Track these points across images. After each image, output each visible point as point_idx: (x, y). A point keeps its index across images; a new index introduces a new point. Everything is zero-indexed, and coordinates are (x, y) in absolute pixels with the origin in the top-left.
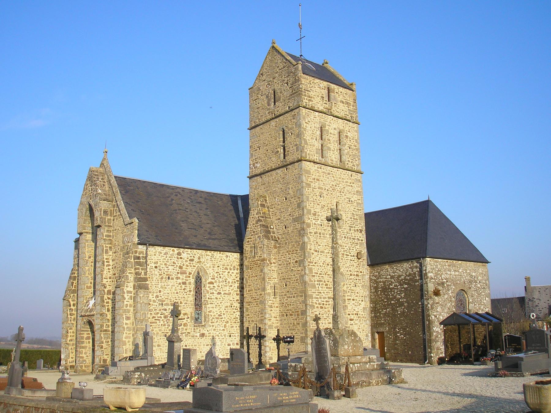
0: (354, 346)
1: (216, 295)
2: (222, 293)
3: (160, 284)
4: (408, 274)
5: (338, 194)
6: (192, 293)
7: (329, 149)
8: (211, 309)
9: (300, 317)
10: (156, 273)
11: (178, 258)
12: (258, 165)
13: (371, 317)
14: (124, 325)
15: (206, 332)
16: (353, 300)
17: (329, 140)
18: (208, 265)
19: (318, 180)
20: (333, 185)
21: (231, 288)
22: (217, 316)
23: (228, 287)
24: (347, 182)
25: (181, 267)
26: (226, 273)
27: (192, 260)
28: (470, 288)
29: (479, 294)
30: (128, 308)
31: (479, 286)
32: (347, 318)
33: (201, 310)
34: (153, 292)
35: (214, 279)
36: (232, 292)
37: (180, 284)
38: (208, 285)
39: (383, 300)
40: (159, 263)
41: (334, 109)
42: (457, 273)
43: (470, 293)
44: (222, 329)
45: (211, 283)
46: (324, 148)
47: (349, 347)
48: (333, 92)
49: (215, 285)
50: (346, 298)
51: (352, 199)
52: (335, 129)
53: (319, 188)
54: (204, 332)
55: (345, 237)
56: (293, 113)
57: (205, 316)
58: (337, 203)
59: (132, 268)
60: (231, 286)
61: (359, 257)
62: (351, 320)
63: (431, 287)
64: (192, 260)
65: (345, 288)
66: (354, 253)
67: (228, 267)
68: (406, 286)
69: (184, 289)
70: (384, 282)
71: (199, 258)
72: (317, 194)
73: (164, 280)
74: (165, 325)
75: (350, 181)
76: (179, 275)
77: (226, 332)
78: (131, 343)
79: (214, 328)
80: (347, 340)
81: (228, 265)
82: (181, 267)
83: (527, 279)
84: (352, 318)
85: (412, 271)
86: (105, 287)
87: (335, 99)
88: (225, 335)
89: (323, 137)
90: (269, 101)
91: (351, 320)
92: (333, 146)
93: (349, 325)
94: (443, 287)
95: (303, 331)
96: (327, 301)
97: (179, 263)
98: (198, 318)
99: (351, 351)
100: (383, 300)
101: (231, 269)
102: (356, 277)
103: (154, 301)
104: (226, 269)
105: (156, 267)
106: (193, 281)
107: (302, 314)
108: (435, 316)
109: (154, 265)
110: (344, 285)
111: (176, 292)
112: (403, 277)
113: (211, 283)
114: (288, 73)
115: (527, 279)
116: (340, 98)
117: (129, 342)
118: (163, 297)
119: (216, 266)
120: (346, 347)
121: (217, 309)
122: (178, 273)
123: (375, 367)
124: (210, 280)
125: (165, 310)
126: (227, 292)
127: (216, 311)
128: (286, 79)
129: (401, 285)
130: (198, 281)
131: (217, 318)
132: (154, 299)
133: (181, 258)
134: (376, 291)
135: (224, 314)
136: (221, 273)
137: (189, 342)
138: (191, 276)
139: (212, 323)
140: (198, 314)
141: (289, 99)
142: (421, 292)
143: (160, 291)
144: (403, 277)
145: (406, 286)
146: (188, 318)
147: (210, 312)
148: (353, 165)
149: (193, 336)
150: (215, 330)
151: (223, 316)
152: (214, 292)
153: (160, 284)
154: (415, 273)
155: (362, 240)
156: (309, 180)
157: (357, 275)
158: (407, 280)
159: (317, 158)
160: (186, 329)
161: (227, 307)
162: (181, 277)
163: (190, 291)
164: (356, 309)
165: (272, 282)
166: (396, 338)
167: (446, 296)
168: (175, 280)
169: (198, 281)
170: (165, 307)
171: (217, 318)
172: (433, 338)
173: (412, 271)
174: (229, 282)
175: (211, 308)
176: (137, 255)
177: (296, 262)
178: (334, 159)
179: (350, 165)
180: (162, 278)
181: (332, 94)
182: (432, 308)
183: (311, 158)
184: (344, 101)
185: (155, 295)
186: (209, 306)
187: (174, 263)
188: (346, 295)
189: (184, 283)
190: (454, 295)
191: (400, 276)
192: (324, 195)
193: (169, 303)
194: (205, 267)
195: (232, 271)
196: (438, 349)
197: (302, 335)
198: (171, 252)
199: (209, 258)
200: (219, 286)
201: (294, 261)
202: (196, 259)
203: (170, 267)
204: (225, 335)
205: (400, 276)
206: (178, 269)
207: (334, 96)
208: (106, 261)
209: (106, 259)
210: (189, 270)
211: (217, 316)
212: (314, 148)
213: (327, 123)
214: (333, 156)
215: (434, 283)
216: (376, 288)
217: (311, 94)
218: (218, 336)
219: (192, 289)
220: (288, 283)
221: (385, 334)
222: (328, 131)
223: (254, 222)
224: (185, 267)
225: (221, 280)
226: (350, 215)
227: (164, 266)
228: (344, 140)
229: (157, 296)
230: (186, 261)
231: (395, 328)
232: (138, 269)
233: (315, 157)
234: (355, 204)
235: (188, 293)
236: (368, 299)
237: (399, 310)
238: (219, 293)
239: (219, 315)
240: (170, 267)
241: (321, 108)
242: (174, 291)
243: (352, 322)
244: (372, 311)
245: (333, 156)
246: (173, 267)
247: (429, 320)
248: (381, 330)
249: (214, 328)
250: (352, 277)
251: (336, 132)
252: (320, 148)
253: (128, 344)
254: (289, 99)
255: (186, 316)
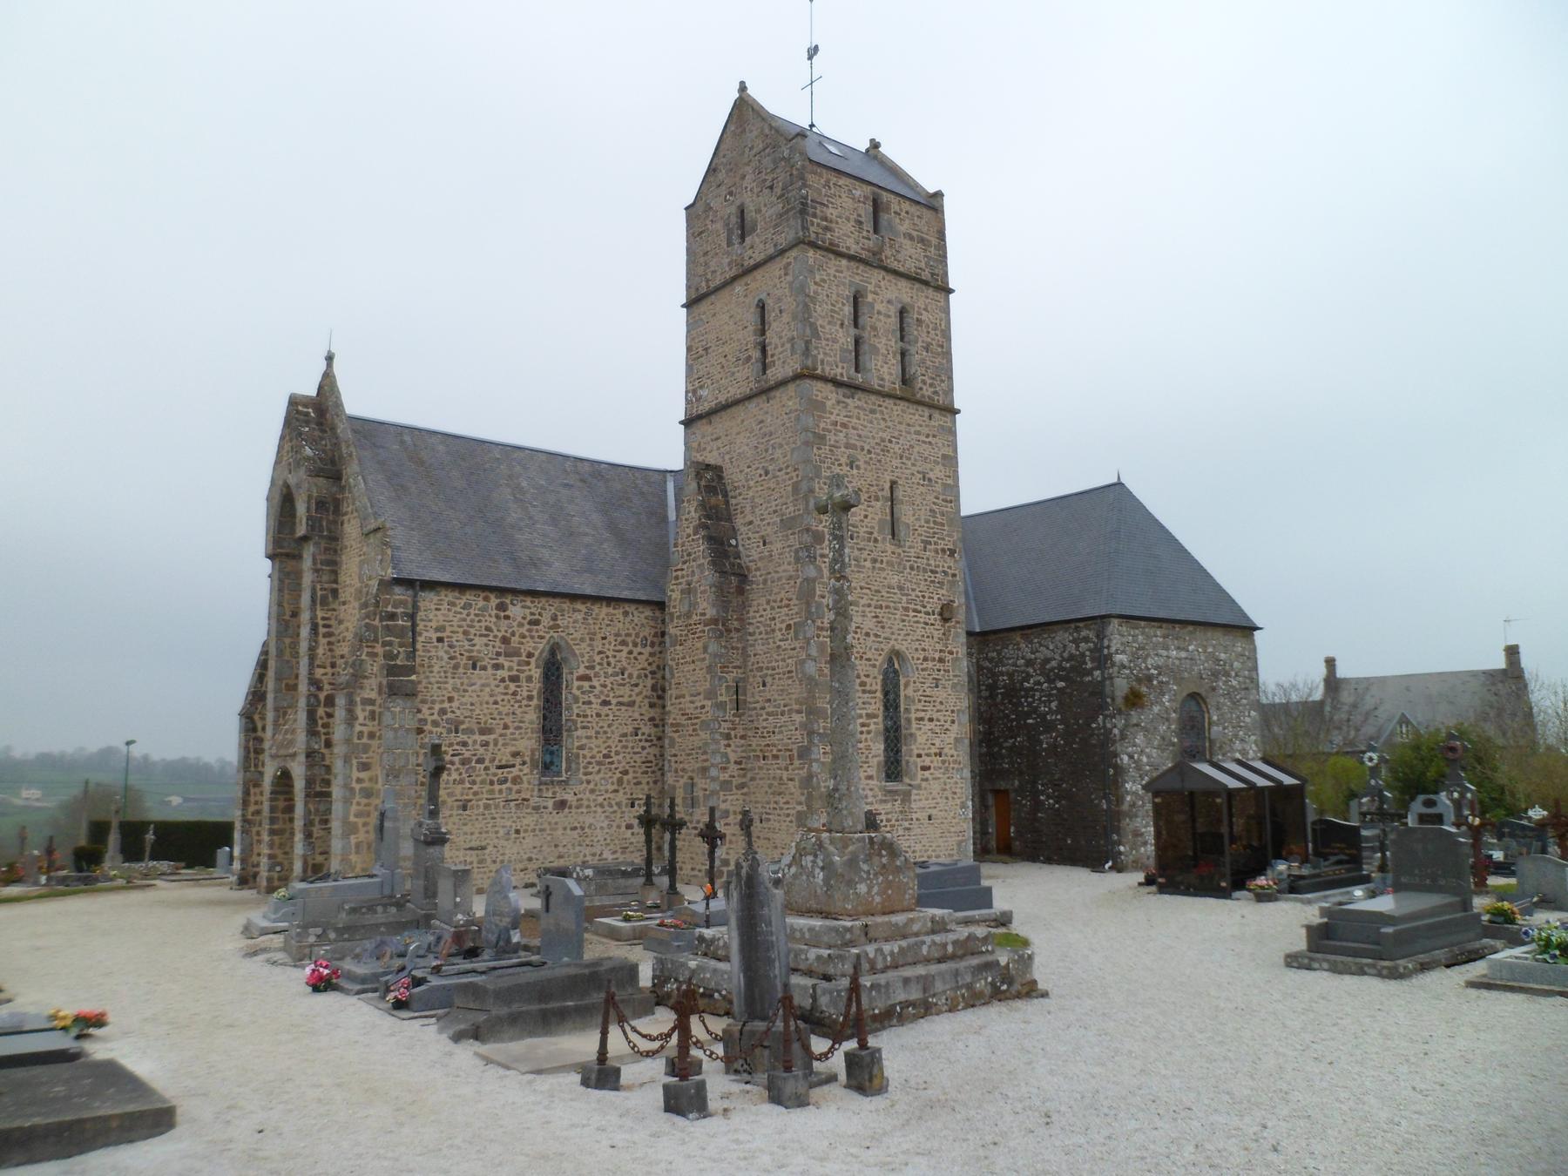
0: (889, 884)
1: (596, 706)
2: (614, 701)
3: (451, 681)
4: (1066, 655)
5: (896, 462)
6: (535, 702)
7: (875, 350)
8: (584, 741)
9: (797, 763)
10: (441, 653)
11: (497, 617)
12: (704, 393)
13: (981, 755)
14: (354, 784)
15: (569, 797)
16: (931, 720)
17: (874, 328)
18: (577, 635)
19: (844, 425)
20: (883, 440)
21: (637, 690)
22: (599, 757)
23: (627, 688)
24: (918, 433)
25: (505, 640)
26: (624, 654)
27: (537, 623)
28: (1214, 689)
29: (1235, 703)
30: (365, 740)
31: (1234, 683)
32: (915, 764)
33: (558, 743)
34: (433, 702)
35: (592, 668)
36: (638, 699)
37: (503, 680)
38: (576, 684)
39: (1007, 716)
40: (449, 629)
41: (888, 252)
42: (1183, 654)
43: (1211, 702)
44: (611, 788)
45: (586, 678)
46: (865, 348)
47: (870, 888)
48: (888, 210)
49: (595, 682)
50: (913, 716)
51: (931, 475)
52: (889, 302)
53: (847, 446)
54: (566, 797)
55: (912, 568)
56: (785, 261)
57: (568, 759)
58: (893, 484)
59: (376, 640)
60: (636, 685)
61: (946, 615)
62: (924, 768)
63: (1121, 686)
64: (537, 623)
65: (910, 691)
66: (934, 605)
67: (629, 640)
68: (1061, 684)
69: (515, 694)
70: (1011, 675)
71: (554, 618)
72: (843, 460)
73: (461, 670)
74: (462, 782)
75: (926, 430)
76: (501, 660)
77: (621, 797)
78: (371, 828)
79: (592, 786)
80: (865, 867)
81: (628, 635)
82: (505, 640)
83: (1330, 663)
84: (927, 763)
85: (1077, 647)
86: (320, 689)
87: (891, 227)
88: (619, 804)
89: (861, 321)
90: (730, 232)
91: (924, 768)
92: (884, 343)
93: (918, 782)
94: (1150, 686)
95: (803, 799)
96: (863, 725)
97: (503, 628)
98: (552, 763)
99: (878, 899)
100: (1007, 716)
101: (635, 645)
102: (939, 666)
103: (435, 724)
104: (624, 643)
105: (440, 640)
106: (536, 673)
107: (800, 757)
108: (1131, 757)
109: (435, 636)
110: (906, 685)
111: (491, 700)
112: (1054, 663)
113: (586, 678)
114: (774, 162)
115: (1330, 663)
116: (905, 227)
117: (365, 824)
118: (458, 713)
119: (599, 636)
120: (862, 888)
121: (600, 741)
122: (498, 654)
123: (950, 949)
124: (582, 671)
125: (465, 744)
126: (626, 700)
127: (596, 747)
128: (769, 178)
129: (1050, 681)
130: (553, 671)
131: (599, 763)
132: (435, 717)
133: (507, 617)
134: (992, 696)
135: (617, 753)
136: (610, 654)
137: (526, 822)
138: (533, 660)
139: (586, 774)
140: (552, 753)
141: (776, 226)
142: (1097, 699)
143: (450, 699)
144: (1054, 663)
145: (1061, 684)
146: (524, 763)
147: (581, 748)
148: (935, 393)
149: (536, 808)
150: (592, 791)
151: (615, 758)
152: (593, 699)
153: (451, 681)
154: (1083, 655)
155: (954, 575)
156: (822, 425)
157: (941, 660)
158: (1064, 669)
159: (843, 371)
160: (519, 792)
161: (625, 735)
162: (506, 664)
163: (530, 698)
164: (937, 742)
165: (729, 677)
166: (1038, 805)
167: (1156, 709)
168: (490, 671)
169: (553, 671)
170: (465, 738)
171: (599, 763)
172: (1125, 807)
173: (1077, 647)
174: (630, 676)
175: (582, 740)
176: (390, 609)
177: (789, 627)
178: (887, 377)
179: (927, 391)
180: (456, 667)
181: (884, 217)
182: (1123, 737)
183: (829, 371)
184: (915, 234)
185: (437, 707)
186: (580, 732)
187: (488, 629)
188: (913, 708)
189: (514, 679)
190: (1176, 705)
191: (1047, 661)
192: (861, 463)
193: (475, 727)
194: (569, 638)
195: (639, 649)
196: (1137, 834)
197: (799, 808)
198: (481, 603)
199: (579, 616)
200: (604, 686)
201: (784, 626)
202: (546, 621)
203: (477, 640)
204: (619, 804)
205: (1047, 661)
206: (498, 644)
207: (889, 222)
208: (321, 623)
209: (323, 619)
210: (529, 646)
211: (599, 757)
212: (836, 346)
213: (870, 288)
214: (885, 369)
215: (1128, 677)
216: (992, 688)
217: (831, 212)
218: (601, 805)
219: (535, 693)
220: (769, 680)
221: (1012, 795)
222: (872, 305)
223: (690, 531)
224: (516, 639)
225: (610, 671)
226: (924, 514)
227: (461, 636)
228: (913, 331)
229: (443, 712)
230: (521, 625)
231: (1034, 783)
232: (390, 644)
233: (839, 370)
234: (938, 488)
235: (525, 702)
236: (965, 718)
237: (1045, 741)
238: (605, 703)
239: (605, 756)
240: (477, 640)
241: (854, 249)
242: (487, 698)
243: (927, 773)
244: (981, 742)
245: (883, 370)
246: (485, 640)
247: (1117, 767)
248: (1002, 785)
249: (592, 786)
250: (930, 664)
251: (893, 311)
252: (851, 347)
253: (362, 830)
254: (776, 226)
255: (519, 760)
